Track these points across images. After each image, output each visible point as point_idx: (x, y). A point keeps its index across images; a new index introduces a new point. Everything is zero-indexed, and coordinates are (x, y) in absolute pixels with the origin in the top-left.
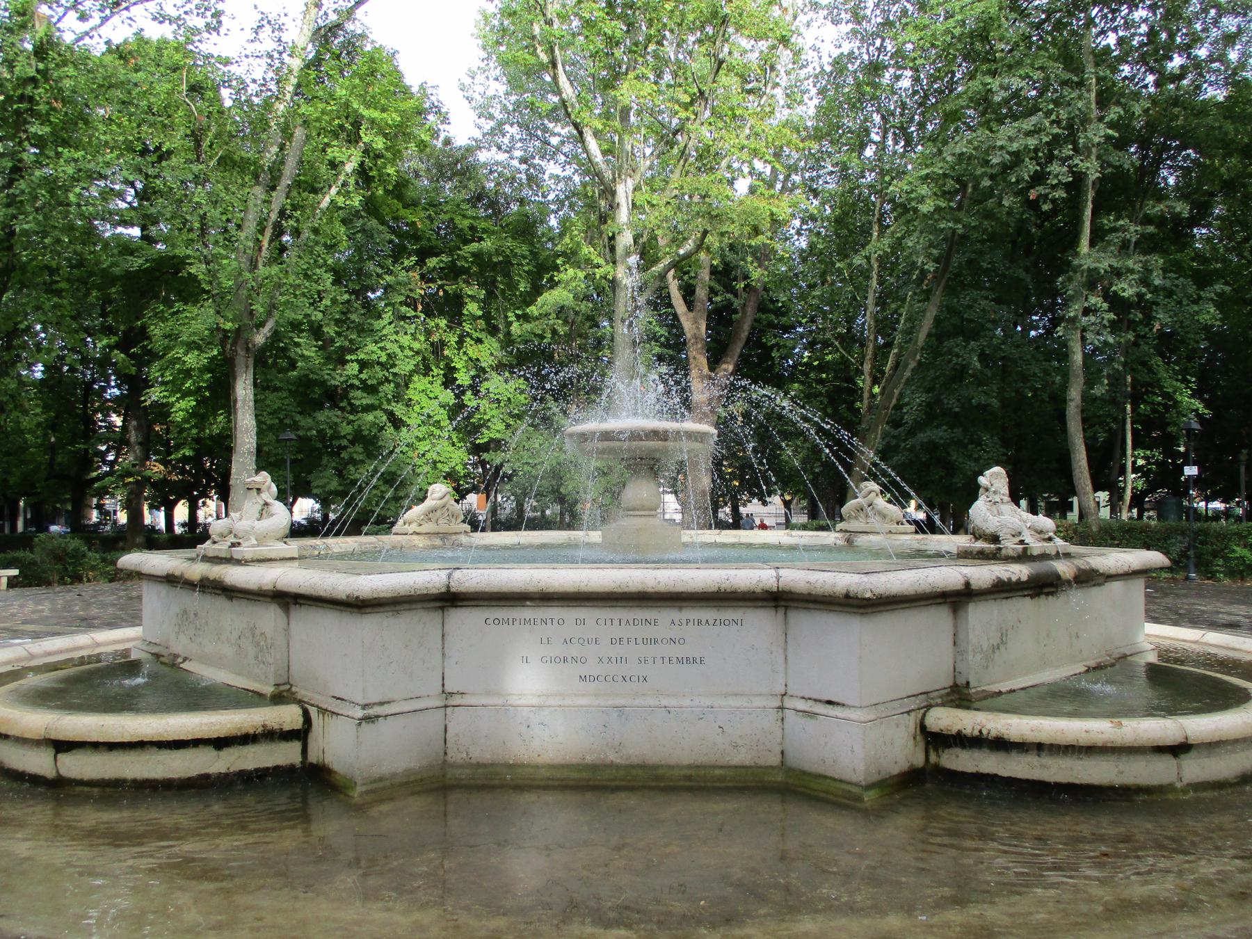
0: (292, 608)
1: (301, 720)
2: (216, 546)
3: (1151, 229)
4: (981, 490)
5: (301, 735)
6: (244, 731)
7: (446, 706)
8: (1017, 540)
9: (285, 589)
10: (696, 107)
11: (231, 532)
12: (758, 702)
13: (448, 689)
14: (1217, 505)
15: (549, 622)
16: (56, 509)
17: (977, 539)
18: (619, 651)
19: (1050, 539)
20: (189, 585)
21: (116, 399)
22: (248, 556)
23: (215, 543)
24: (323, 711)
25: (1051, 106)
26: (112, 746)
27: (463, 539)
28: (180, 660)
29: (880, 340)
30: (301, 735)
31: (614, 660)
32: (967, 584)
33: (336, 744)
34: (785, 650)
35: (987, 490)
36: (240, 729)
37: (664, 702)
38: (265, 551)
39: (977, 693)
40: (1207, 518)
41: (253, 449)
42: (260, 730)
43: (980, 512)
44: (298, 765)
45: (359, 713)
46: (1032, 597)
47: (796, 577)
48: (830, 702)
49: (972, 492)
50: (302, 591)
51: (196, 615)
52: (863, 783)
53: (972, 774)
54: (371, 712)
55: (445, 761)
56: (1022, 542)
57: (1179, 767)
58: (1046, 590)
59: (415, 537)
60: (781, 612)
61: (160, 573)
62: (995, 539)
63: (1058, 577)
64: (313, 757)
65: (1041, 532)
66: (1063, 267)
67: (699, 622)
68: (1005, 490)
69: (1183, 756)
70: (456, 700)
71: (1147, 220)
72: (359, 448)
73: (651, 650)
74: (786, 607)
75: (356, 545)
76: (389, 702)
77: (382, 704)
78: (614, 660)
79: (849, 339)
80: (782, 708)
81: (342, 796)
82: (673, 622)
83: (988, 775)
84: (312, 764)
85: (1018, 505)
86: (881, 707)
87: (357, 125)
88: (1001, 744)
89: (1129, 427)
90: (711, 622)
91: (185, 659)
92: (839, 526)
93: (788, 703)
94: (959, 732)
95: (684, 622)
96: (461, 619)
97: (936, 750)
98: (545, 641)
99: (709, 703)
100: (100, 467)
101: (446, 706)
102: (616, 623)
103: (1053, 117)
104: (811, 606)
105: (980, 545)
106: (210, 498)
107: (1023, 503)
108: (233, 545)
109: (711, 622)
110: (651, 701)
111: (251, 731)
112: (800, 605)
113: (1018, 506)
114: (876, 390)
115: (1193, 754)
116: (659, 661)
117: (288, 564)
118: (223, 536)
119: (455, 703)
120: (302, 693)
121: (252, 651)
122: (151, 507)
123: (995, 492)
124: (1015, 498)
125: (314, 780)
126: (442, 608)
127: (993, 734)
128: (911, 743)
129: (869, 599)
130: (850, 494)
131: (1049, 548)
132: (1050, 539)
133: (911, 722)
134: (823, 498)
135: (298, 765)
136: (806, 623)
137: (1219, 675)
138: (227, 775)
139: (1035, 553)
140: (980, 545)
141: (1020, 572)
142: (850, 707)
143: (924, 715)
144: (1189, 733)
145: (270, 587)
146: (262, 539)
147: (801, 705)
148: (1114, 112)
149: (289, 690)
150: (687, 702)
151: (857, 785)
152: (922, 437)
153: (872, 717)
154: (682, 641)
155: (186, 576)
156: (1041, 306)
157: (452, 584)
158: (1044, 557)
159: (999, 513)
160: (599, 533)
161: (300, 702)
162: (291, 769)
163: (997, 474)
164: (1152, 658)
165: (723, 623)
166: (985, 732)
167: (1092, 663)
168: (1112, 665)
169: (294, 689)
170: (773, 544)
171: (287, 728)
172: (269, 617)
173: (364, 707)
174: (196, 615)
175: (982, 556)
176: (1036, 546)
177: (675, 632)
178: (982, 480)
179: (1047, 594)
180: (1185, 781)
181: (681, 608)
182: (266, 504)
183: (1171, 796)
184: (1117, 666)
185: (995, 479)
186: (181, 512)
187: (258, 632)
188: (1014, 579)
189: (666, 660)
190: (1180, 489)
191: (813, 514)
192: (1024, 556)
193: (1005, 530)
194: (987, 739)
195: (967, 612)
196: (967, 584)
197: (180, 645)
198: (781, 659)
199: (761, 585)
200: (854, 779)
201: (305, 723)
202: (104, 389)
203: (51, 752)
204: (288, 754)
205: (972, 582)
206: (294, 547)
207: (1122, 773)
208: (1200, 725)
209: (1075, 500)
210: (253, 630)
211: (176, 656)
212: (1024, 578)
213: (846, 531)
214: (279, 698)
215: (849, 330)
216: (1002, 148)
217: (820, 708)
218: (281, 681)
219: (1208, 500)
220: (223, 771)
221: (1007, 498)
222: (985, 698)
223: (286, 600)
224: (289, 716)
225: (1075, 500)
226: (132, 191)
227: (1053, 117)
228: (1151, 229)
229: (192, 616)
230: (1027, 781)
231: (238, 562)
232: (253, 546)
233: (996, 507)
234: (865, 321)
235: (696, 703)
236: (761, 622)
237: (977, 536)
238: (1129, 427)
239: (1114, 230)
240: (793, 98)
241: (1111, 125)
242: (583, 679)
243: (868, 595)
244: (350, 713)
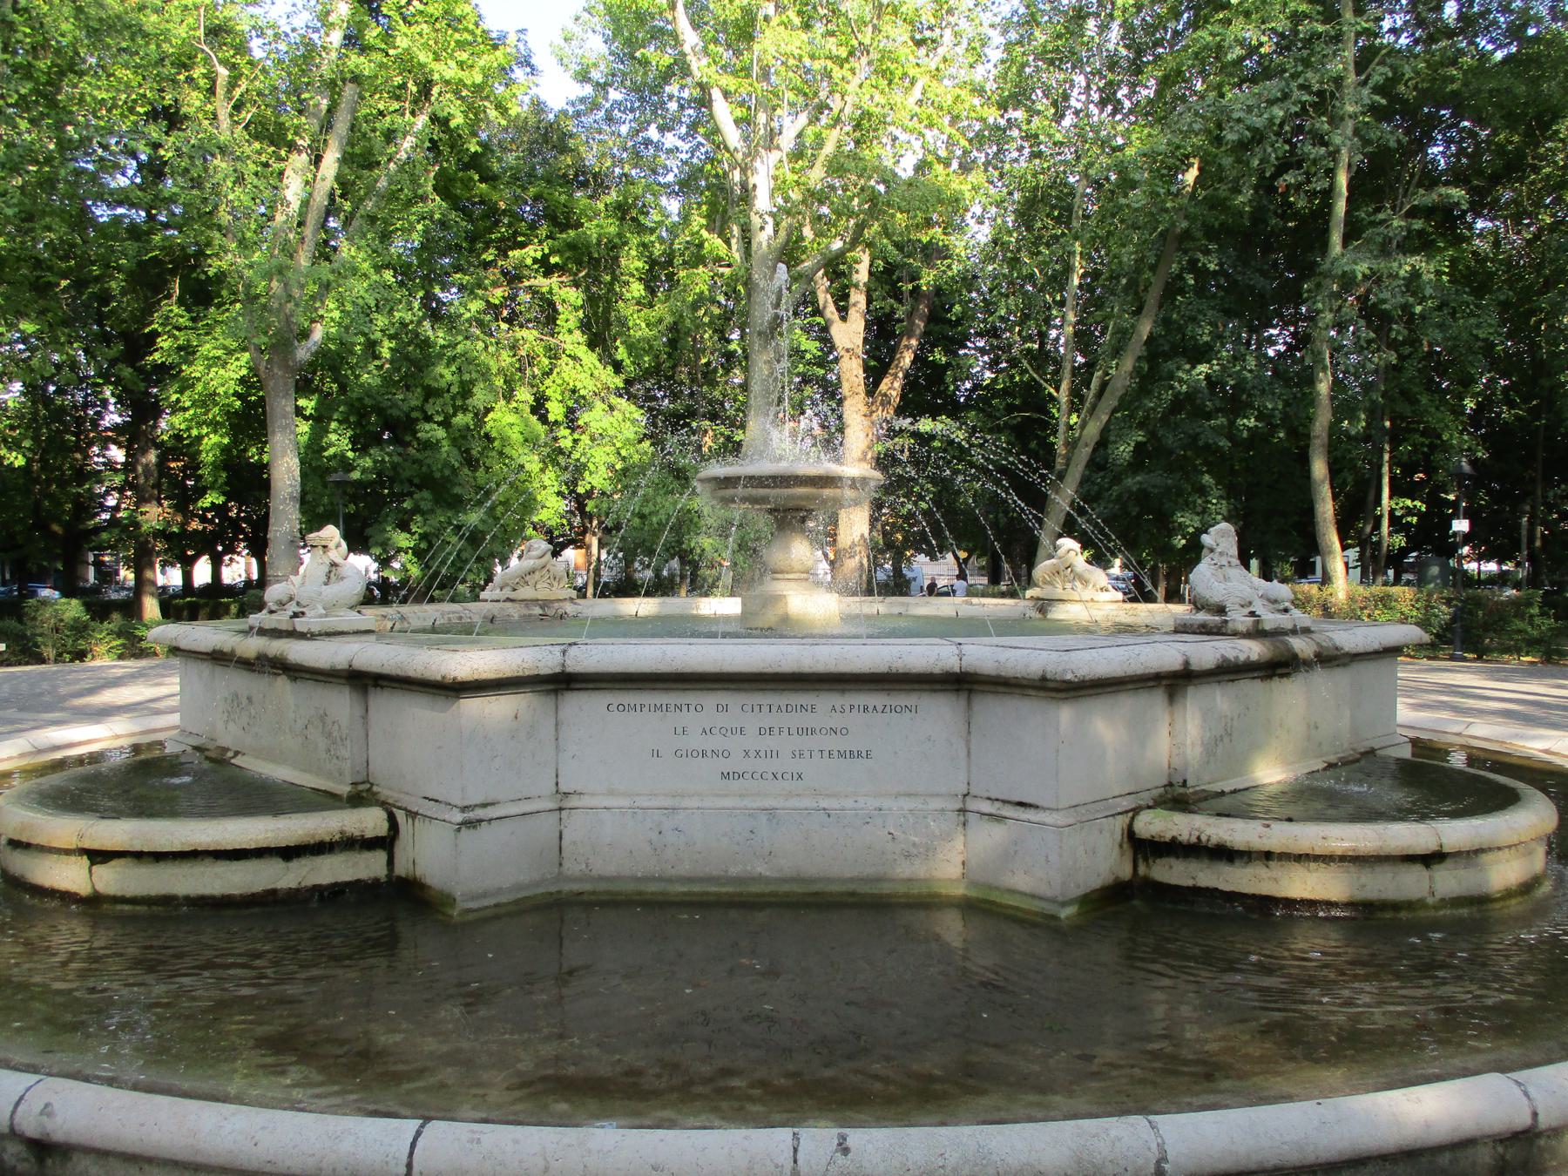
0: (371, 690)
1: (386, 825)
2: (274, 616)
3: (1418, 225)
4: (1205, 551)
5: (386, 843)
6: (318, 839)
7: (561, 809)
8: (1246, 611)
9: (364, 668)
10: (853, 63)
11: (291, 599)
12: (937, 804)
13: (563, 788)
14: (1492, 567)
15: (685, 708)
16: (41, 567)
17: (1198, 609)
18: (769, 742)
19: (1286, 610)
20: (247, 664)
21: (116, 428)
22: (315, 629)
23: (272, 612)
24: (413, 815)
25: (1300, 68)
26: (159, 857)
27: (569, 608)
28: (230, 754)
29: (1080, 359)
30: (386, 843)
31: (762, 754)
32: (1187, 663)
33: (428, 853)
34: (968, 742)
35: (1212, 550)
36: (313, 836)
37: (824, 803)
38: (333, 622)
39: (1195, 793)
40: (1480, 582)
41: (297, 494)
42: (337, 837)
43: (1207, 578)
44: (383, 879)
45: (459, 817)
46: (1262, 678)
47: (982, 655)
48: (1021, 804)
49: (1194, 551)
50: (386, 670)
51: (249, 699)
52: (1060, 899)
53: (1188, 888)
54: (471, 815)
55: (560, 873)
56: (1252, 614)
57: (1431, 878)
58: (1279, 671)
59: (509, 604)
60: (964, 696)
61: (203, 649)
62: (1221, 610)
63: (1295, 656)
64: (401, 869)
65: (1275, 602)
66: (1308, 270)
67: (866, 709)
68: (1234, 551)
69: (1436, 867)
70: (573, 802)
71: (1413, 213)
72: (426, 494)
73: (807, 742)
74: (970, 691)
75: (438, 615)
76: (493, 804)
77: (484, 805)
78: (762, 754)
79: (1043, 358)
80: (963, 811)
81: (440, 917)
82: (834, 708)
83: (1207, 889)
84: (399, 878)
85: (1247, 567)
86: (1082, 810)
87: (426, 88)
88: (1224, 854)
89: (1385, 469)
90: (880, 708)
91: (237, 753)
92: (1029, 593)
93: (972, 805)
94: (1174, 839)
95: (847, 708)
96: (577, 705)
97: (1146, 860)
98: (679, 730)
99: (877, 804)
100: (98, 514)
101: (561, 809)
102: (765, 709)
103: (1301, 81)
104: (1001, 689)
105: (1202, 617)
106: (239, 554)
107: (1254, 563)
108: (295, 615)
109: (880, 708)
110: (807, 802)
111: (327, 839)
112: (986, 688)
113: (1247, 567)
114: (1074, 419)
115: (1449, 863)
116: (816, 755)
117: (364, 638)
118: (281, 604)
119: (571, 805)
120: (385, 793)
121: (322, 743)
122: (164, 564)
123: (1221, 554)
124: (1245, 561)
125: (406, 897)
126: (556, 692)
127: (1214, 840)
128: (1117, 850)
129: (1069, 682)
130: (1041, 553)
131: (1284, 621)
132: (1286, 610)
133: (1122, 821)
134: (1007, 554)
135: (383, 879)
136: (992, 709)
137: (1482, 773)
138: (297, 890)
139: (1267, 627)
140: (1202, 617)
141: (1253, 650)
142: (1045, 809)
143: (1133, 819)
144: (1444, 841)
145: (345, 666)
146: (330, 608)
147: (986, 807)
148: (1379, 73)
149: (369, 790)
150: (849, 803)
151: (1052, 900)
152: (1132, 482)
153: (1071, 821)
154: (844, 732)
155: (239, 653)
156: (1281, 317)
157: (568, 662)
158: (1277, 633)
159: (1226, 579)
160: (739, 600)
161: (384, 804)
162: (375, 884)
163: (1223, 534)
164: (1406, 753)
165: (893, 710)
166: (1204, 838)
167: (1333, 759)
168: (1357, 761)
169: (375, 789)
170: (952, 615)
171: (369, 834)
172: (341, 703)
173: (464, 809)
174: (249, 699)
175: (1205, 630)
176: (1271, 619)
177: (836, 721)
178: (1206, 539)
179: (1282, 676)
180: (1438, 896)
181: (843, 691)
182: (334, 565)
183: (1422, 914)
184: (1363, 762)
185: (1222, 537)
186: (202, 573)
187: (329, 720)
188: (1242, 658)
189: (826, 754)
190: (1446, 547)
191: (995, 577)
192: (1257, 633)
193: (1232, 599)
194: (1206, 847)
195: (1185, 697)
196: (1187, 663)
197: (227, 735)
198: (963, 754)
199: (940, 664)
200: (1049, 893)
201: (390, 829)
202: (100, 415)
203: (85, 861)
204: (371, 866)
205: (1192, 661)
206: (371, 616)
207: (1364, 886)
208: (1455, 832)
209: (1318, 559)
210: (323, 718)
211: (227, 750)
212: (1254, 657)
213: (1038, 599)
214: (360, 798)
215: (1042, 345)
216: (1239, 120)
217: (1008, 811)
218: (360, 779)
219: (1480, 558)
220: (293, 885)
221: (1236, 561)
222: (1206, 799)
223: (362, 681)
224: (371, 821)
225: (1318, 559)
226: (134, 163)
227: (1301, 81)
228: (1418, 225)
229: (245, 701)
230: (1254, 896)
231: (302, 636)
232: (321, 616)
233: (1222, 573)
234: (1061, 335)
235: (861, 804)
236: (939, 711)
237: (1199, 605)
238: (1385, 469)
239: (1373, 224)
240: (977, 50)
241: (1377, 90)
242: (726, 776)
243: (1069, 677)
244: (447, 817)
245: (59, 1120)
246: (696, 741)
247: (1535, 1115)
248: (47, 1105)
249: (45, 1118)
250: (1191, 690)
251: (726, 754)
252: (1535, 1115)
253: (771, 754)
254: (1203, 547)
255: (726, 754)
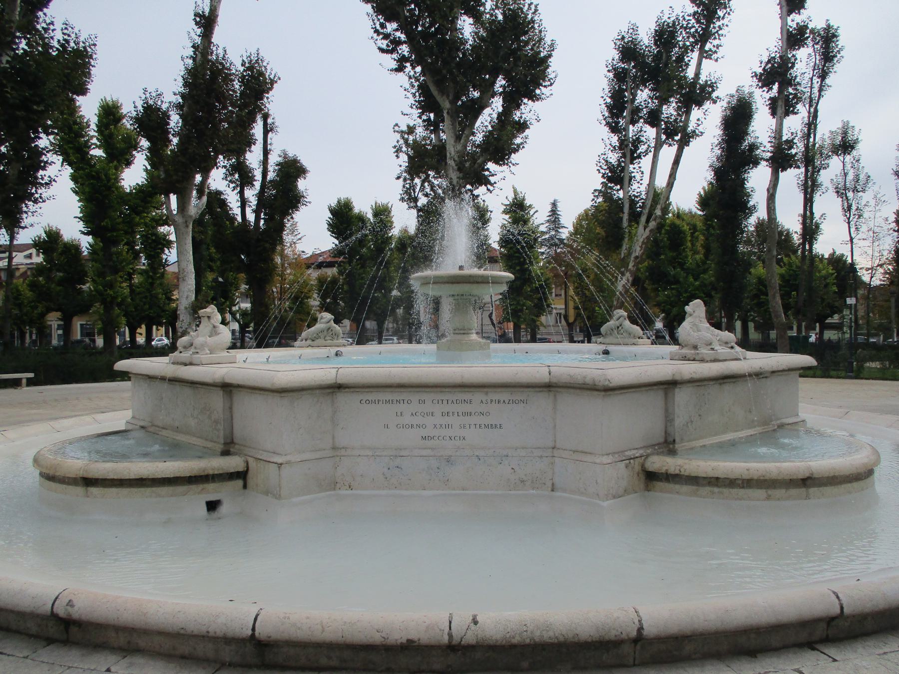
65: (727, 343)
73: (467, 420)
90: (507, 402)
98: (399, 414)
109: (507, 402)
116: (473, 427)
132: (732, 347)
153: (609, 461)
189: (478, 426)
236: (541, 402)
242: (424, 438)
245: (76, 608)
246: (407, 419)
247: (842, 608)
248: (70, 601)
249: (69, 608)
250: (677, 390)
251: (424, 426)
252: (842, 608)
253: (448, 426)
254: (686, 313)
255: (424, 426)
